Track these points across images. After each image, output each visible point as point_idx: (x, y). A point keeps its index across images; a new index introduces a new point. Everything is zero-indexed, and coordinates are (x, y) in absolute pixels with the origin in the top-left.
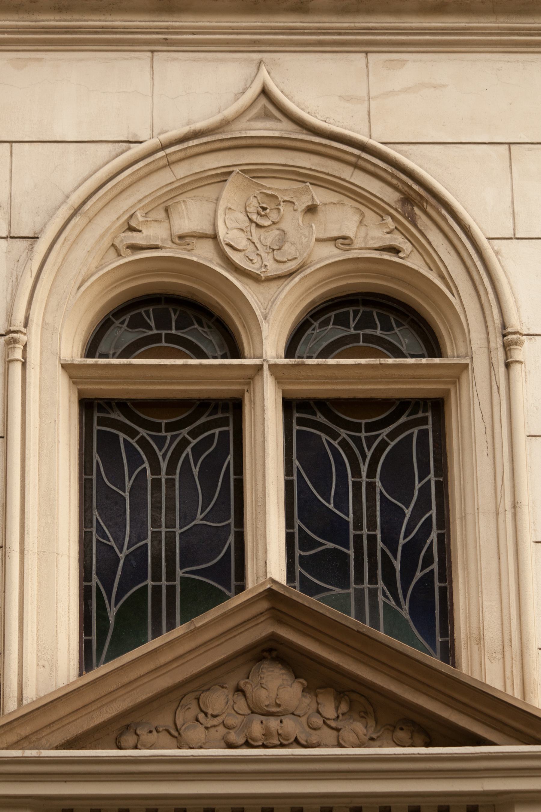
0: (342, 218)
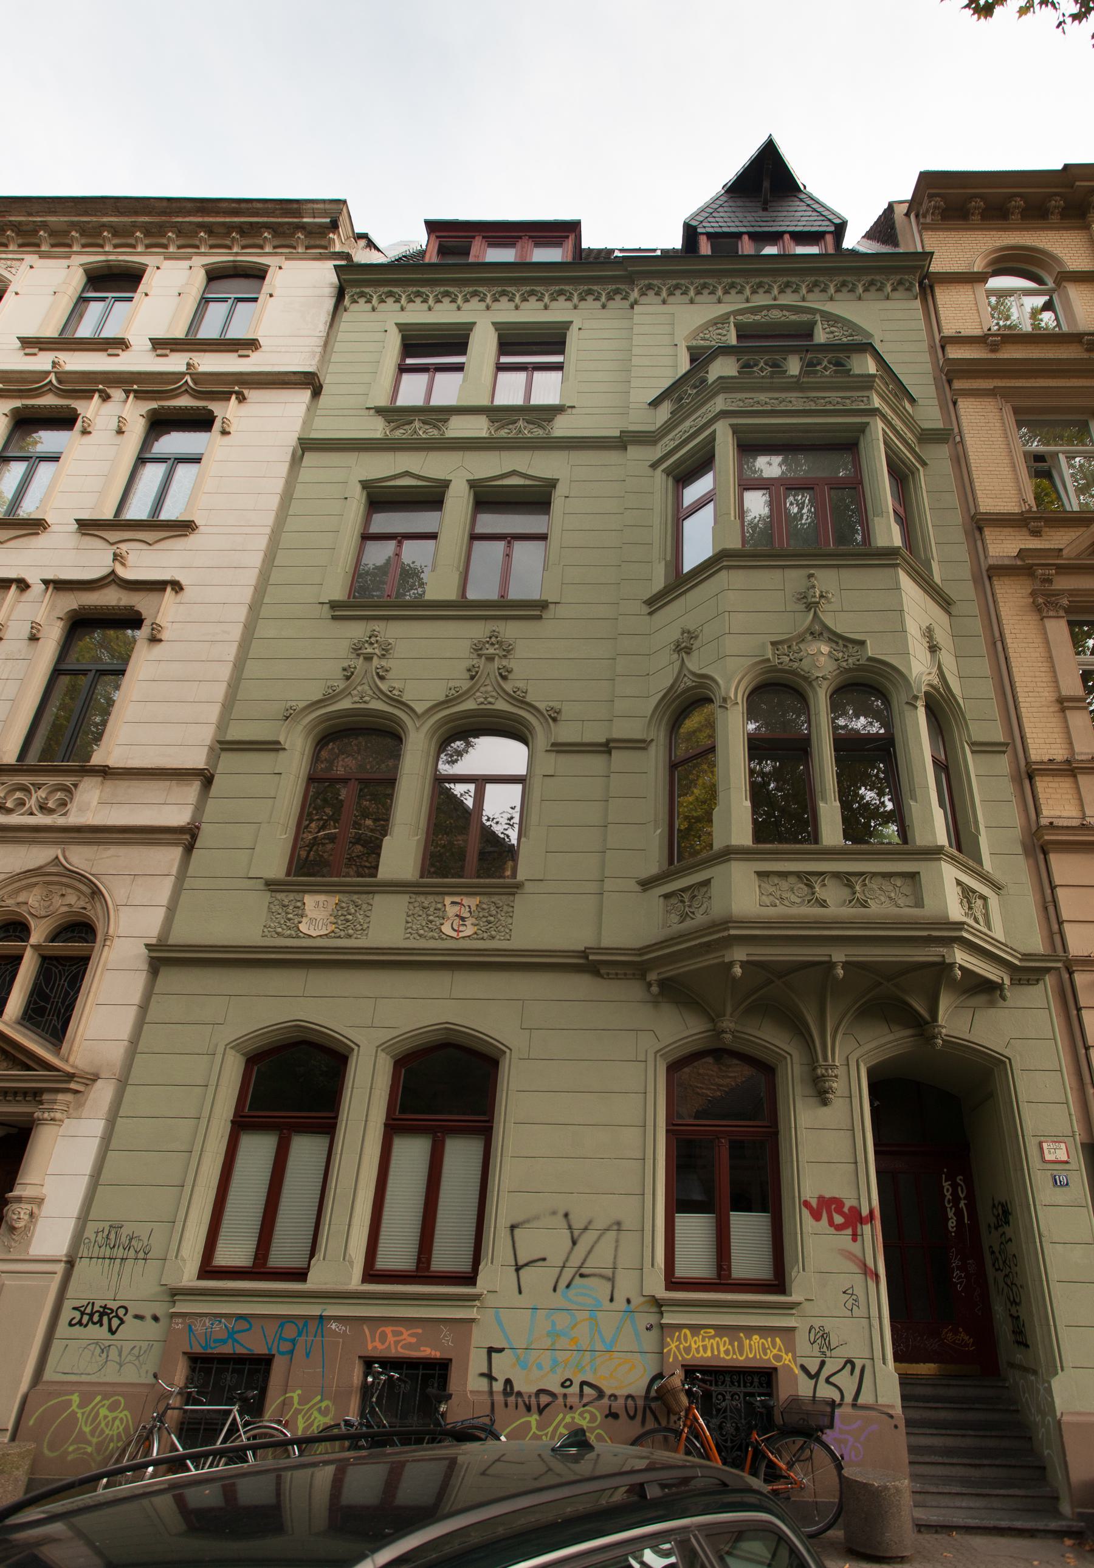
0: (72, 899)
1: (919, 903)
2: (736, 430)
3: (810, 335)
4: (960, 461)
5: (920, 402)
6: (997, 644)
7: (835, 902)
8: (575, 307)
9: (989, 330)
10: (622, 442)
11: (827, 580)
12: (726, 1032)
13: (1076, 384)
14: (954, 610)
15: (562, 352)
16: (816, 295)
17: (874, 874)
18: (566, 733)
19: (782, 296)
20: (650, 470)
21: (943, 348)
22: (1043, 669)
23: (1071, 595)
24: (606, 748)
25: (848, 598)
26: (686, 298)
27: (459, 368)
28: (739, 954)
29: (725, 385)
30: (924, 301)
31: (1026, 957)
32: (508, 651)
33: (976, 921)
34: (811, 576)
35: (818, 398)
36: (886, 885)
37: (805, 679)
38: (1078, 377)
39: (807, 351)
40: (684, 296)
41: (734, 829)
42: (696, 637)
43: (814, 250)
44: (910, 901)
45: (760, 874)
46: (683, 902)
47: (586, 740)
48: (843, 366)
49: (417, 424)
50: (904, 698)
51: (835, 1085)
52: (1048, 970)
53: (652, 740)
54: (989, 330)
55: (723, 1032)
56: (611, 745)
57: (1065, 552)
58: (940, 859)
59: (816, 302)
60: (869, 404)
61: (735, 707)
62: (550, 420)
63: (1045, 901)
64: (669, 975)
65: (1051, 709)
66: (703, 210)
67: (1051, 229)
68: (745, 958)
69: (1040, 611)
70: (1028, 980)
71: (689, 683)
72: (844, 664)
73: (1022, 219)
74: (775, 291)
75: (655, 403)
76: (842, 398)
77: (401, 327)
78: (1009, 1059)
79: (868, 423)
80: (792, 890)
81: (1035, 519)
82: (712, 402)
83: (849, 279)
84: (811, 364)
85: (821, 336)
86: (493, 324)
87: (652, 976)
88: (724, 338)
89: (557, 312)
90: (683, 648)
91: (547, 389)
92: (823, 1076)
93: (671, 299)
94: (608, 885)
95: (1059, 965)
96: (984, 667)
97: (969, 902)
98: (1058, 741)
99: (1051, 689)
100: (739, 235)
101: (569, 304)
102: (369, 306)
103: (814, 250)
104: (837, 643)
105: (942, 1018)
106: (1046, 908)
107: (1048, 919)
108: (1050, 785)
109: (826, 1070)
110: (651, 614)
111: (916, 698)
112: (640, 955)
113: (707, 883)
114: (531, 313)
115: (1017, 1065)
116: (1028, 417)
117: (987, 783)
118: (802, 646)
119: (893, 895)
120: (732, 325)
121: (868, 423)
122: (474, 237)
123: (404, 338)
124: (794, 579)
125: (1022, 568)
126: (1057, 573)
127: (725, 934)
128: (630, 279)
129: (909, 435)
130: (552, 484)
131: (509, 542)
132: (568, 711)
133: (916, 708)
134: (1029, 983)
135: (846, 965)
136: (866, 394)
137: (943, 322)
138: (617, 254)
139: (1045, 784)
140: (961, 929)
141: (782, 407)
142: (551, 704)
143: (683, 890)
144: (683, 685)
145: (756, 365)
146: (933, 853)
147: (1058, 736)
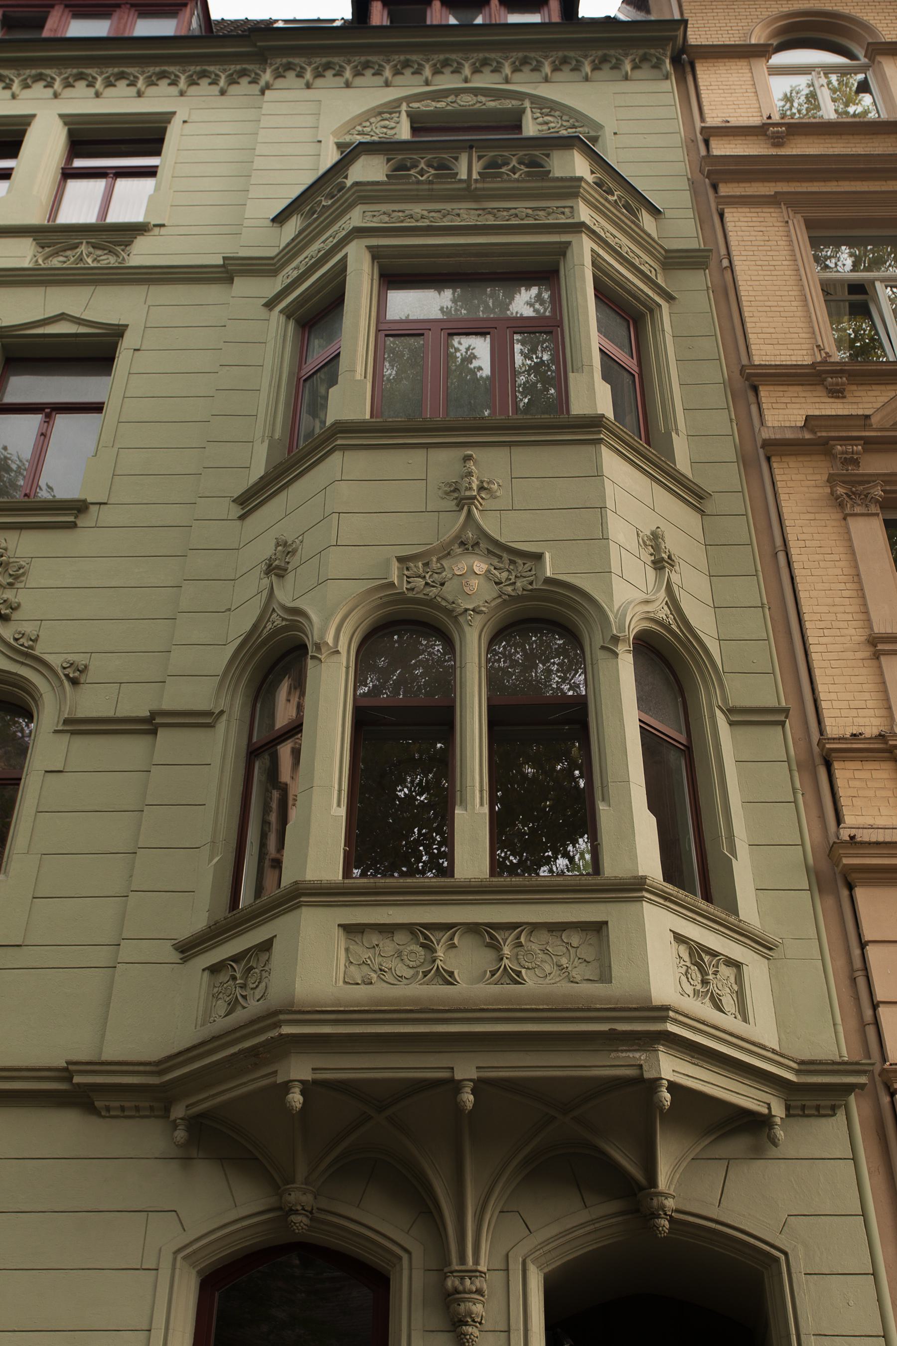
1: (605, 976)
2: (376, 254)
3: (518, 127)
4: (728, 294)
5: (668, 214)
6: (778, 557)
7: (468, 974)
8: (182, 94)
9: (769, 118)
10: (227, 272)
11: (491, 465)
12: (296, 1212)
13: (872, 189)
14: (709, 507)
15: (157, 153)
16: (526, 74)
17: (534, 927)
18: (92, 703)
19: (477, 77)
20: (265, 310)
21: (707, 143)
22: (846, 593)
24: (149, 725)
25: (519, 494)
26: (340, 81)
27: (150, 172)
28: (300, 1069)
29: (367, 193)
30: (681, 80)
31: (806, 1066)
32: (16, 577)
33: (718, 1006)
34: (467, 458)
35: (499, 210)
36: (555, 945)
37: (449, 612)
39: (471, 147)
40: (338, 79)
41: (312, 852)
42: (294, 552)
44: (589, 971)
45: (350, 930)
46: (234, 978)
47: (122, 713)
48: (542, 167)
49: (83, 248)
50: (598, 641)
51: (478, 1309)
52: (849, 1089)
53: (222, 712)
54: (769, 118)
55: (292, 1211)
56: (158, 720)
57: (874, 420)
58: (640, 899)
59: (525, 84)
60: (573, 217)
61: (335, 658)
62: (128, 244)
63: (852, 970)
64: (204, 1107)
65: (860, 655)
68: (308, 1076)
69: (841, 505)
70: (803, 1107)
71: (279, 623)
72: (509, 589)
74: (467, 71)
75: (280, 219)
76: (430, 211)
77: (66, 119)
78: (786, 1254)
79: (569, 243)
80: (400, 954)
81: (841, 372)
82: (348, 217)
83: (571, 54)
84: (493, 165)
85: (531, 128)
86: (61, 116)
87: (178, 1112)
88: (393, 132)
89: (154, 100)
90: (275, 570)
91: (131, 201)
92: (457, 1291)
93: (319, 82)
94: (128, 951)
95: (863, 1080)
96: (750, 591)
97: (703, 972)
98: (870, 704)
99: (860, 624)
101: (174, 90)
102: (91, 91)
104: (500, 557)
105: (663, 1180)
106: (854, 980)
107: (857, 998)
108: (858, 774)
109: (462, 1279)
110: (242, 518)
111: (616, 640)
112: (160, 1073)
113: (267, 946)
114: (119, 101)
115: (799, 1265)
116: (823, 234)
117: (746, 778)
118: (445, 563)
119: (564, 961)
120: (404, 115)
121: (569, 243)
122: (52, 6)
123: (71, 134)
124: (442, 463)
127: (274, 1033)
128: (262, 58)
129: (646, 258)
130: (118, 332)
131: (48, 416)
132: (99, 667)
133: (616, 655)
134: (819, 1113)
135: (480, 1086)
136: (569, 203)
137: (706, 109)
138: (280, 25)
139: (849, 774)
140: (665, 1019)
141: (446, 223)
142: (71, 658)
143: (236, 959)
144: (269, 626)
145: (415, 166)
146: (632, 889)
147: (870, 699)
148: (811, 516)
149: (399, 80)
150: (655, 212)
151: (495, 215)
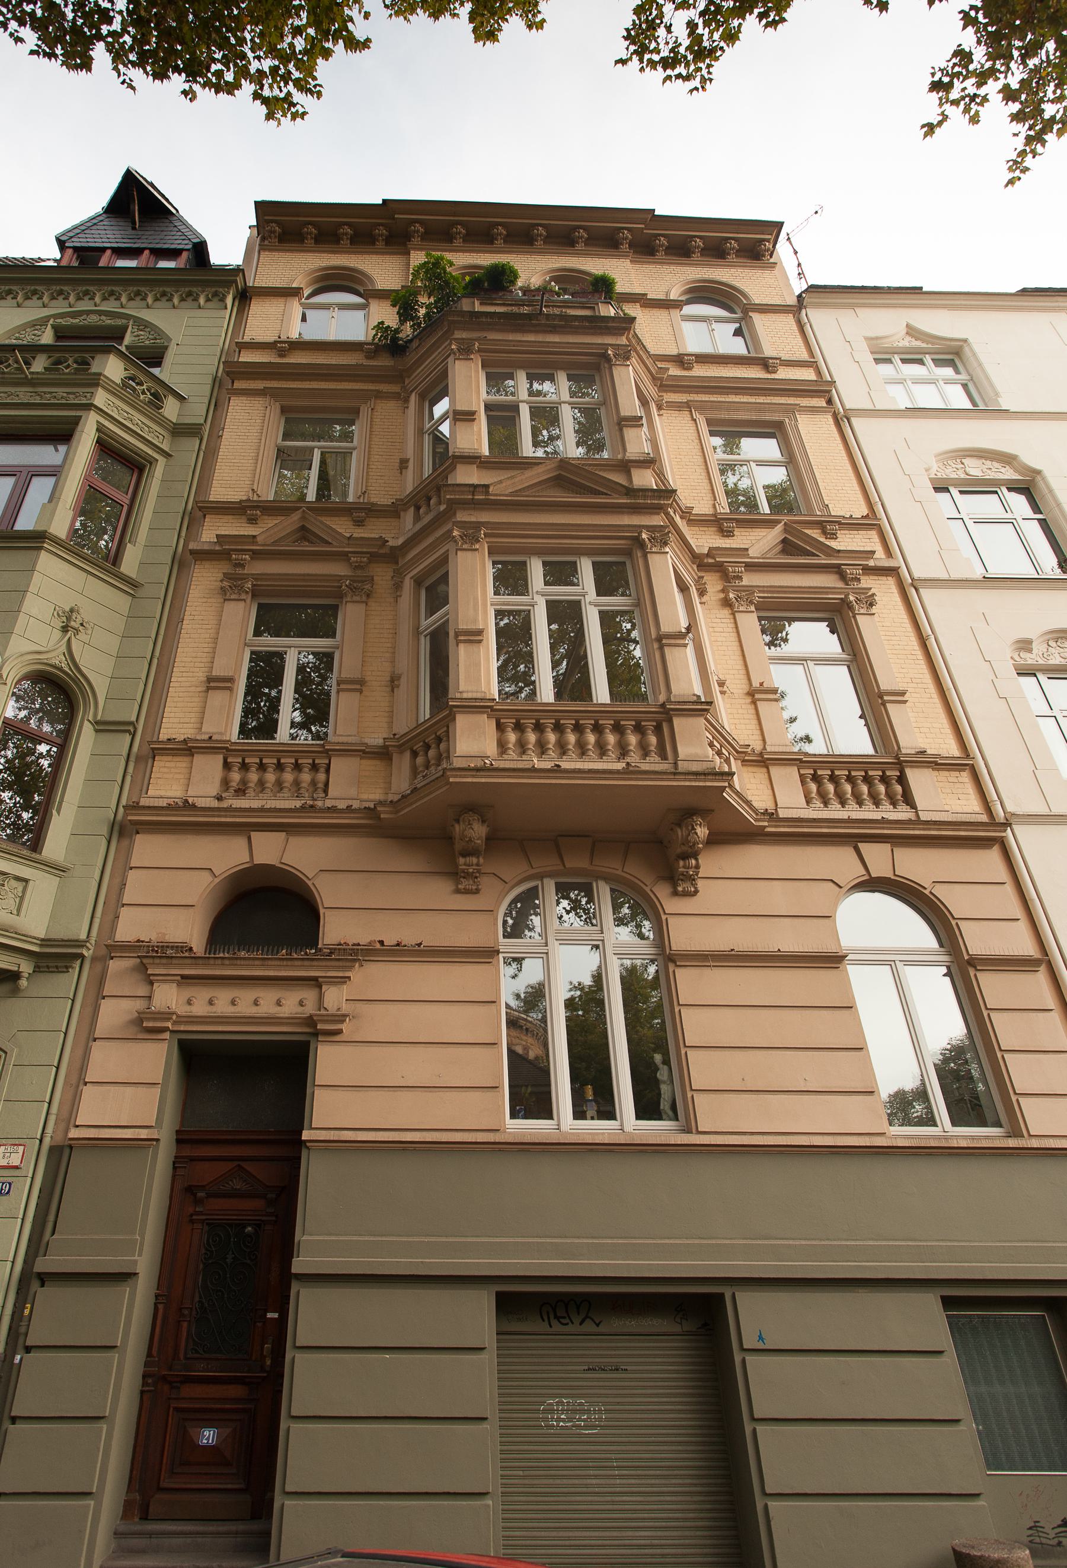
16: (138, 302)
23: (256, 579)
35: (45, 393)
38: (350, 381)
43: (132, 264)
57: (258, 539)
66: (76, 227)
67: (377, 253)
73: (386, 244)
76: (68, 393)
100: (103, 250)
103: (132, 264)
125: (223, 552)
126: (864, 574)
148: (205, 600)
149: (54, 303)
150: (181, 398)
151: (41, 397)
